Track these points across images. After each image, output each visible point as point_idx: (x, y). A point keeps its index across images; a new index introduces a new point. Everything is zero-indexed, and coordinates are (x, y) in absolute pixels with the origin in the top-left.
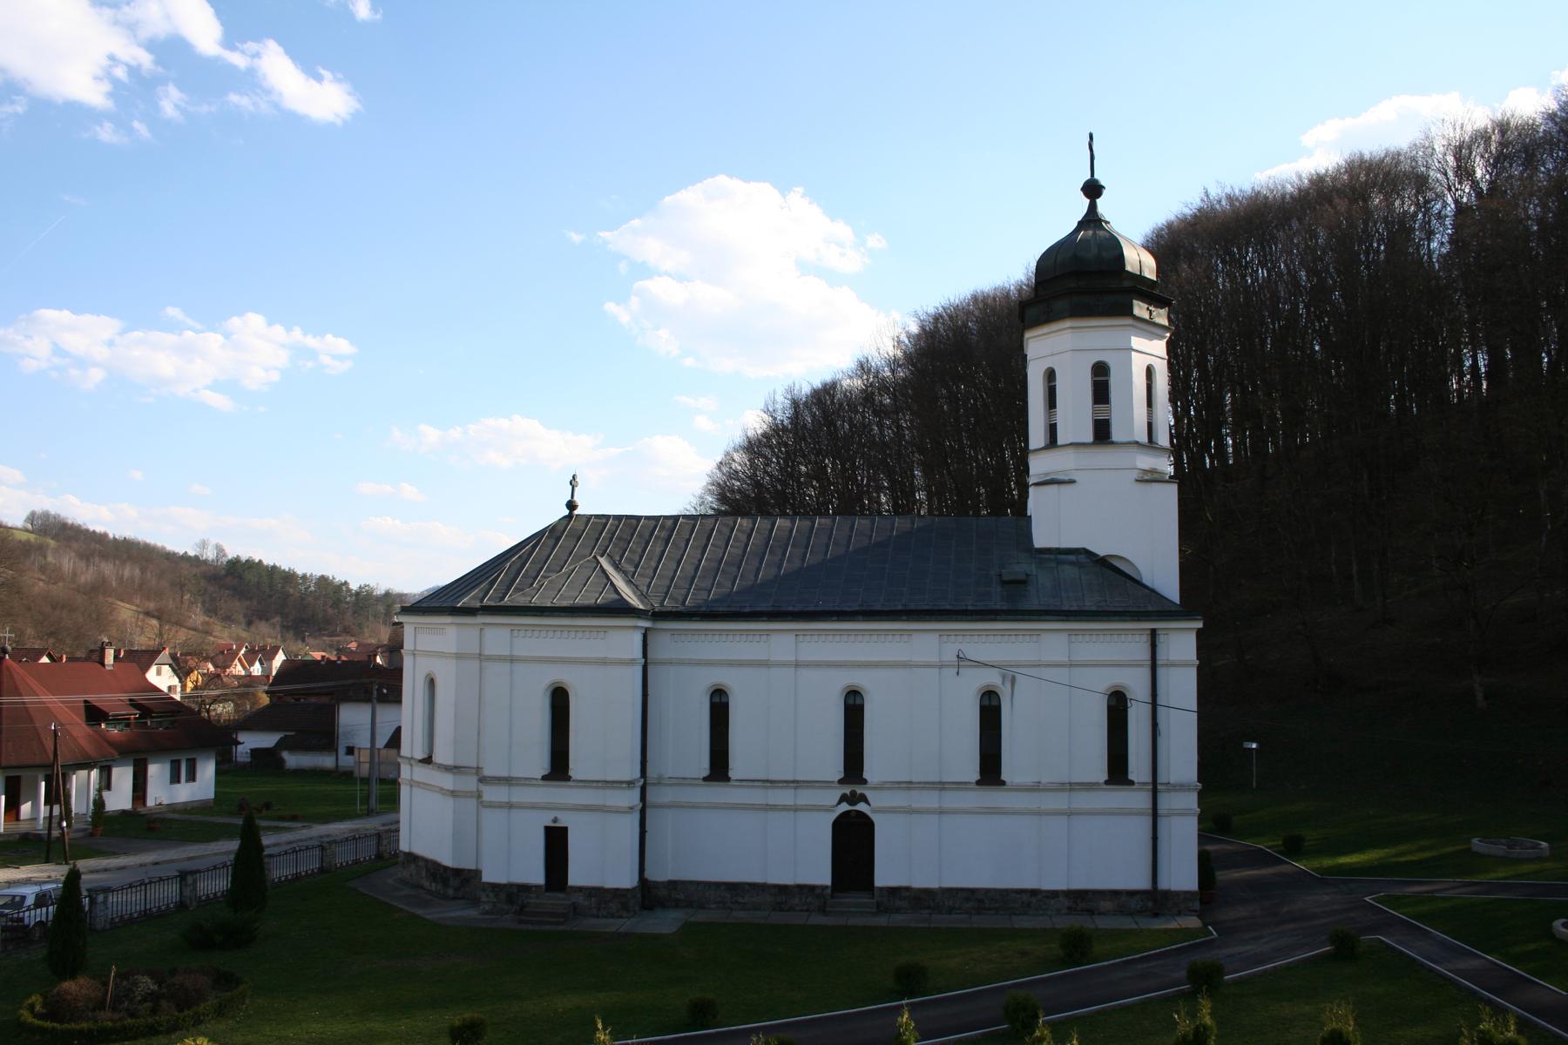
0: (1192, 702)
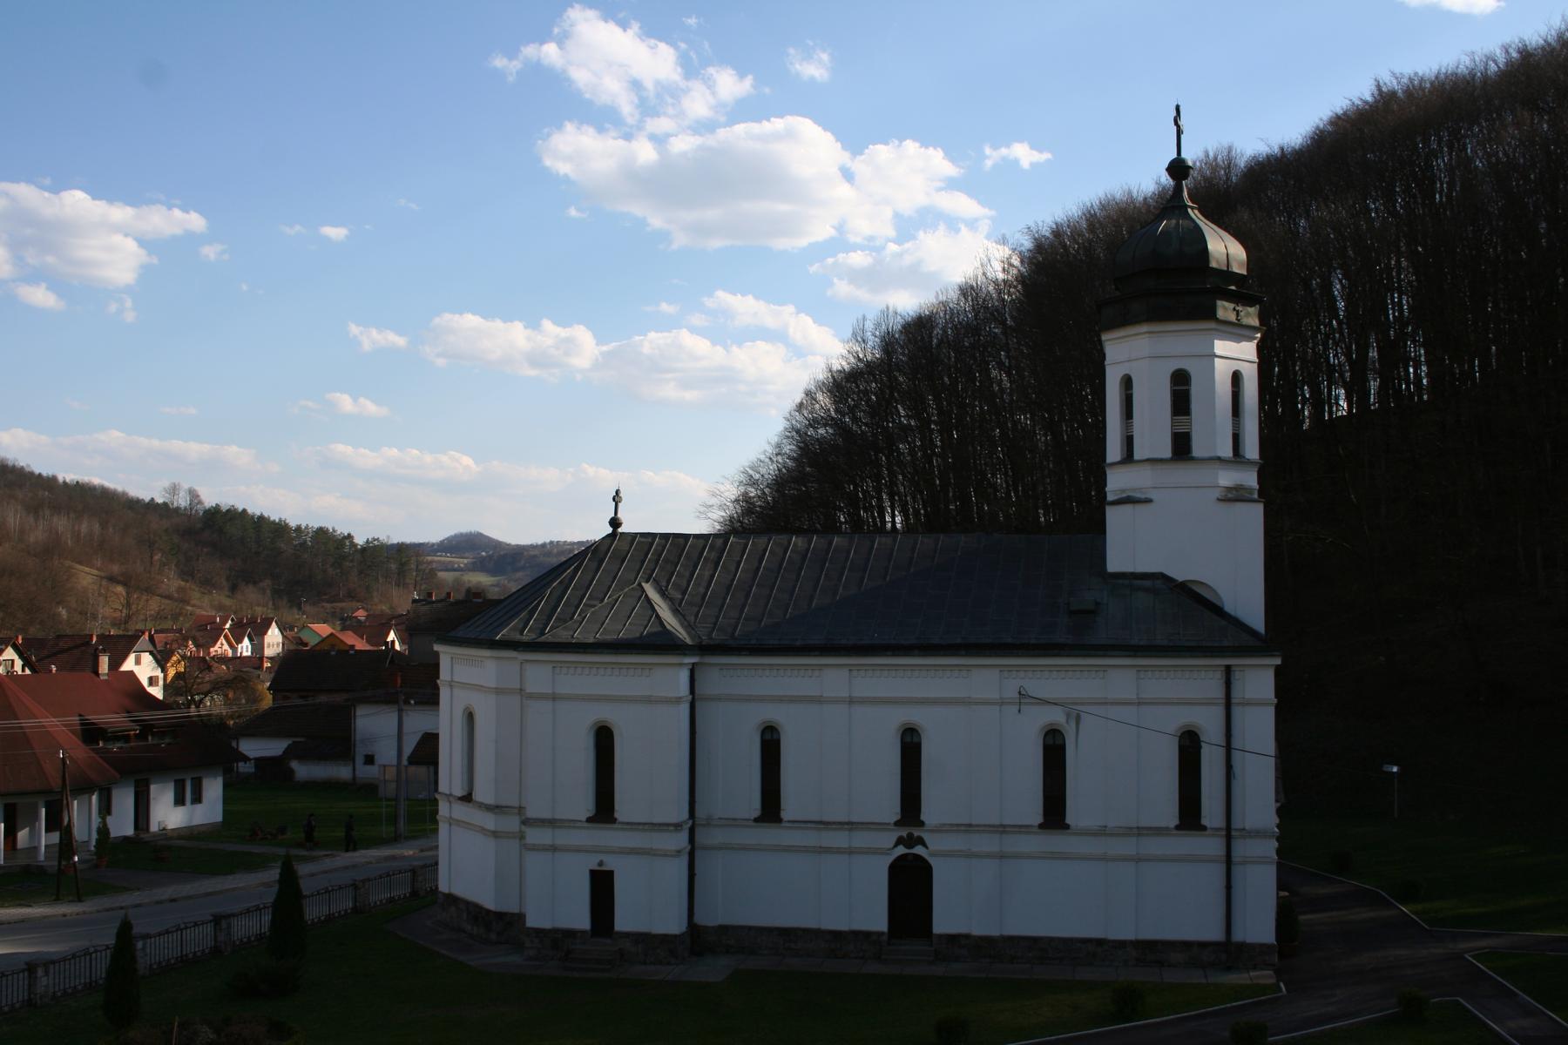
0: (1270, 746)
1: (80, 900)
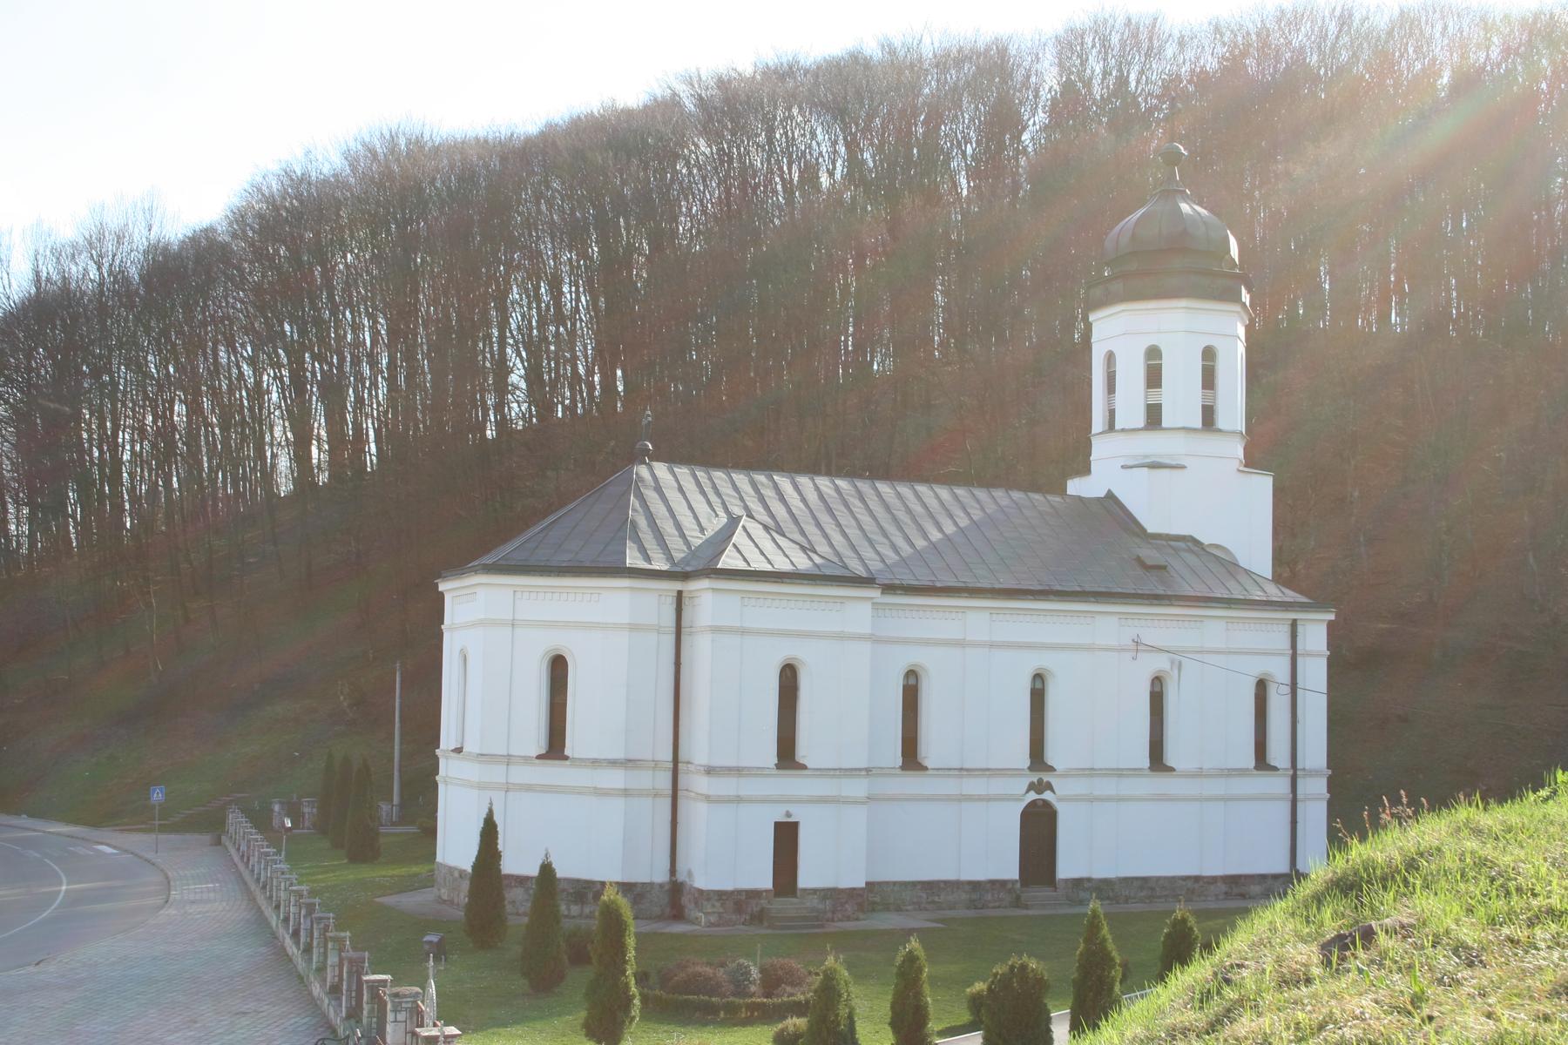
0: (1322, 685)
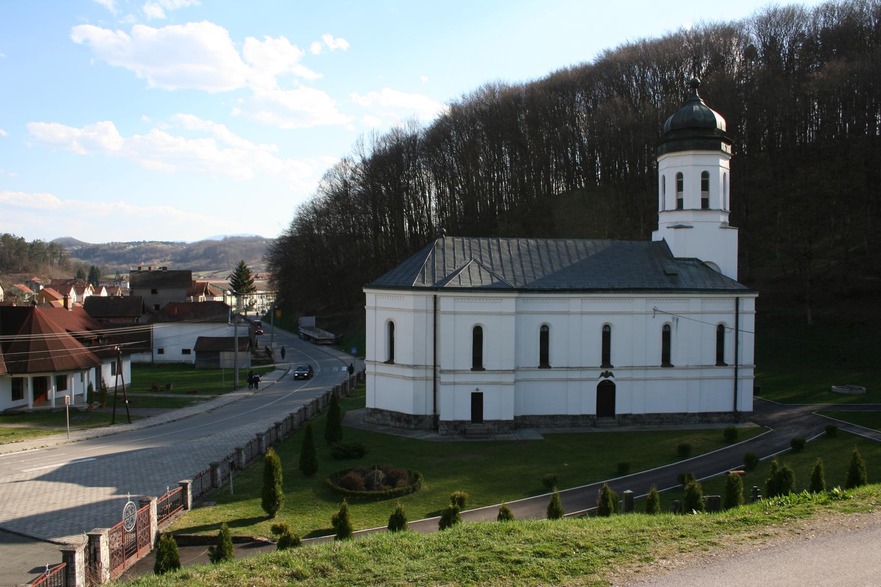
0: (752, 328)
1: (130, 423)
